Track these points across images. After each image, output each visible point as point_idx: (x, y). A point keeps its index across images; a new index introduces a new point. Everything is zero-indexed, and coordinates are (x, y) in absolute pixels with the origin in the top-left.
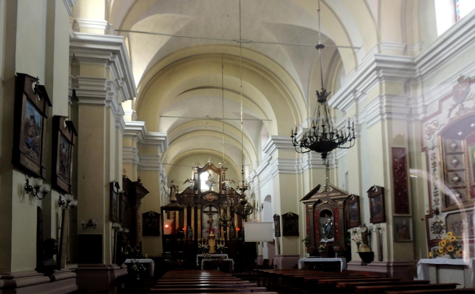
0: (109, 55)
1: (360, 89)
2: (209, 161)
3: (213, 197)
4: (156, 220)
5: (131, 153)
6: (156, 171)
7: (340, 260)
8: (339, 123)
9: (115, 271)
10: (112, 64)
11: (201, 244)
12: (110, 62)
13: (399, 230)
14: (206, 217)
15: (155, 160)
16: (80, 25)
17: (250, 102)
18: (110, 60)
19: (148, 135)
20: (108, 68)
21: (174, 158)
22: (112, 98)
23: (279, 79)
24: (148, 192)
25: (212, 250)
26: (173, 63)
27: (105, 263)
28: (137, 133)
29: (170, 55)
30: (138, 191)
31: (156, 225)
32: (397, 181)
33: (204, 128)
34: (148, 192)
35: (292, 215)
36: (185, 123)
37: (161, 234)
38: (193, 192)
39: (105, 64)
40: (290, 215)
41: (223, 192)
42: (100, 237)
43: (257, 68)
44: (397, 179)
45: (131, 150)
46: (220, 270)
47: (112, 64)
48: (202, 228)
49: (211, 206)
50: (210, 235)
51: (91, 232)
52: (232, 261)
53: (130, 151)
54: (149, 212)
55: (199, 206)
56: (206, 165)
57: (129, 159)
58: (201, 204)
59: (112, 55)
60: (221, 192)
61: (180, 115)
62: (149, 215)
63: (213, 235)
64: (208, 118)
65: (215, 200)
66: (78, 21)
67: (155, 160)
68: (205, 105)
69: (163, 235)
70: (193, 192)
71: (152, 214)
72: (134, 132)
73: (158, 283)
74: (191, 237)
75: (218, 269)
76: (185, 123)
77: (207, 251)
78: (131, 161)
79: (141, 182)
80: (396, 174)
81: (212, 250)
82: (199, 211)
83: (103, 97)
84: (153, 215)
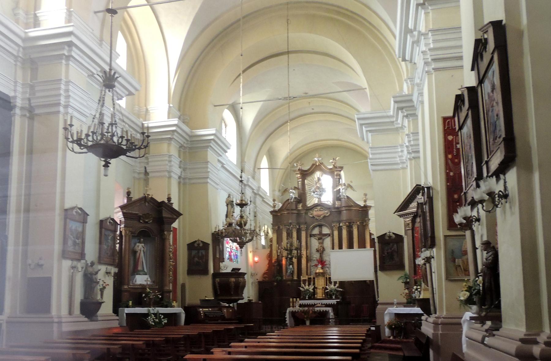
0: (64, 49)
1: (411, 25)
2: (316, 159)
3: (326, 213)
4: (203, 252)
5: (167, 162)
6: (204, 183)
7: (288, 311)
8: (73, 124)
9: (63, 324)
10: (71, 59)
11: (305, 284)
12: (69, 58)
13: (457, 260)
14: (315, 243)
15: (204, 168)
16: (40, 19)
17: (342, 64)
18: (66, 54)
19: (193, 134)
20: (67, 65)
21: (287, 158)
22: (69, 102)
23: (370, 23)
24: (181, 214)
25: (320, 294)
26: (225, 29)
27: (54, 312)
28: (173, 135)
29: (216, 19)
30: (165, 214)
31: (204, 260)
32: (452, 174)
33: (309, 110)
34: (181, 214)
35: (394, 236)
36: (279, 107)
37: (211, 271)
38: (294, 207)
39: (64, 61)
40: (390, 237)
41: (338, 204)
42: (49, 280)
43: (338, 13)
44: (451, 171)
45: (167, 158)
46: (310, 324)
47: (71, 59)
48: (308, 260)
49: (320, 226)
50: (318, 271)
51: (40, 274)
52: (180, 313)
53: (164, 160)
54: (196, 241)
55: (303, 227)
56: (313, 165)
57: (164, 171)
58: (306, 223)
59: (66, 48)
60: (334, 204)
61: (264, 99)
62: (196, 245)
63: (321, 271)
64: (306, 96)
65: (325, 217)
66: (38, 15)
67: (204, 168)
68: (298, 79)
69: (217, 275)
70: (294, 207)
71: (199, 244)
72: (167, 135)
73: (361, 341)
74: (292, 274)
75: (308, 323)
76: (279, 107)
77: (312, 296)
78: (167, 174)
79: (172, 202)
80: (450, 162)
81: (320, 294)
82: (303, 234)
83: (58, 102)
84: (201, 245)
